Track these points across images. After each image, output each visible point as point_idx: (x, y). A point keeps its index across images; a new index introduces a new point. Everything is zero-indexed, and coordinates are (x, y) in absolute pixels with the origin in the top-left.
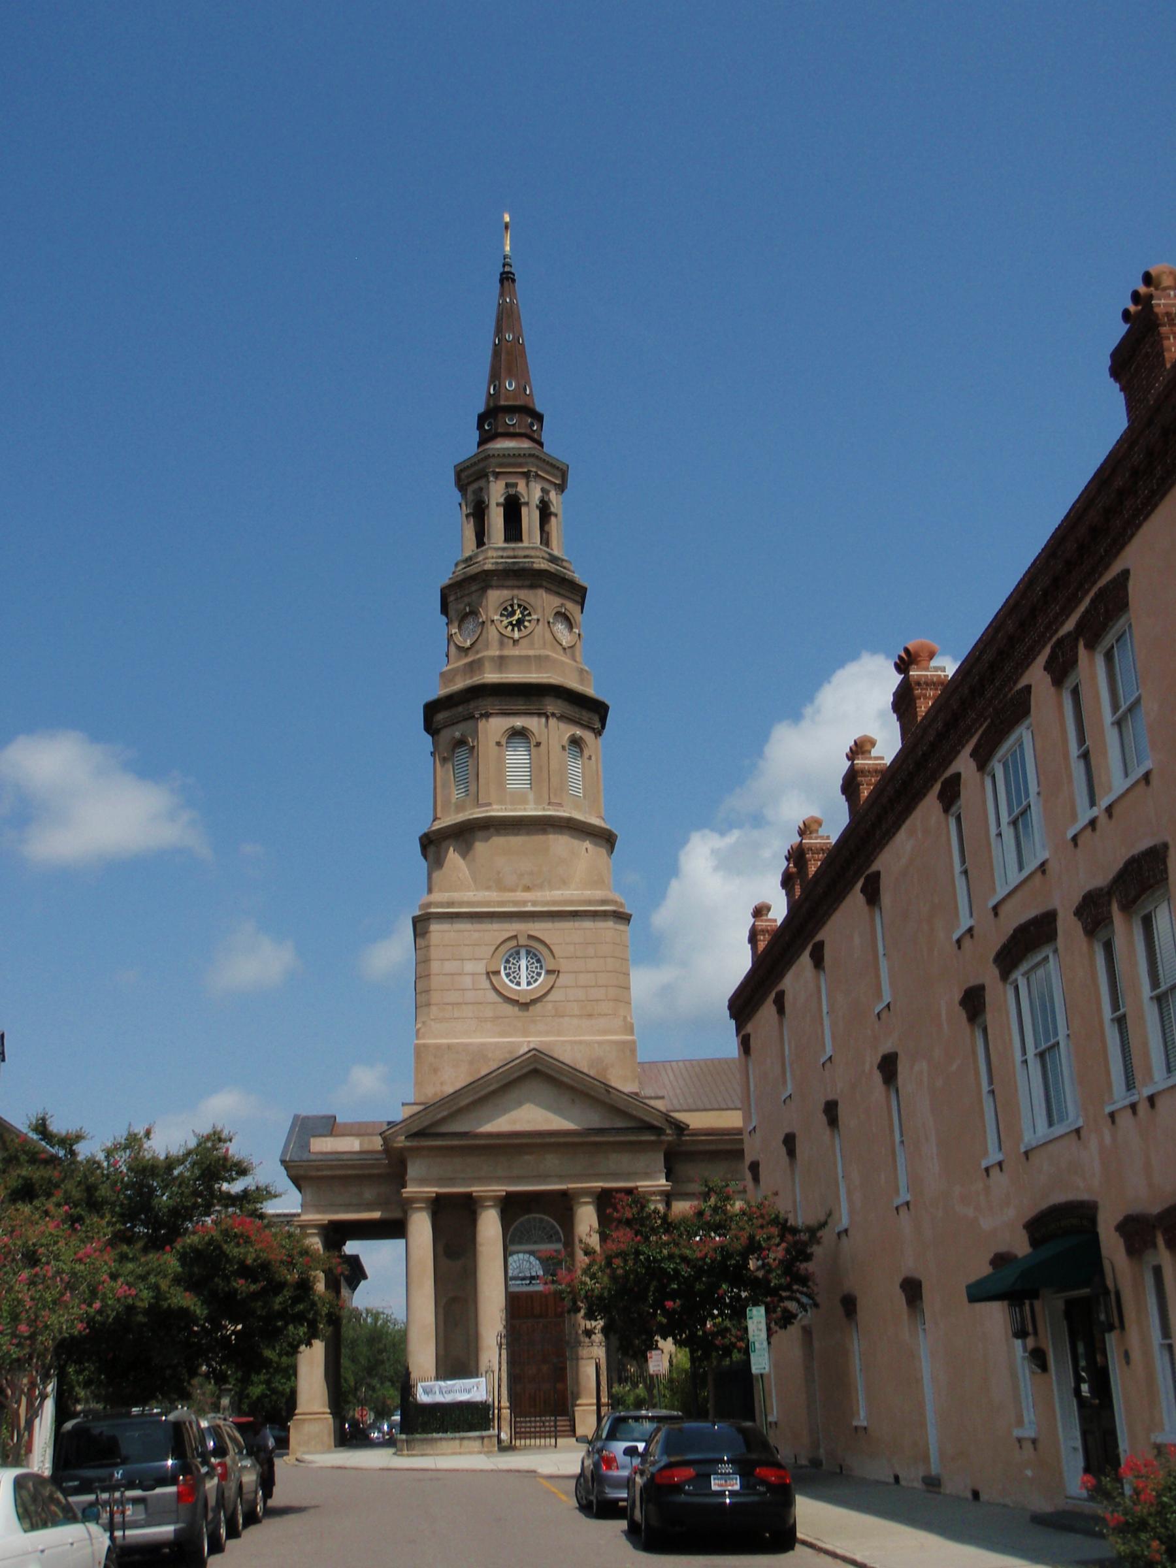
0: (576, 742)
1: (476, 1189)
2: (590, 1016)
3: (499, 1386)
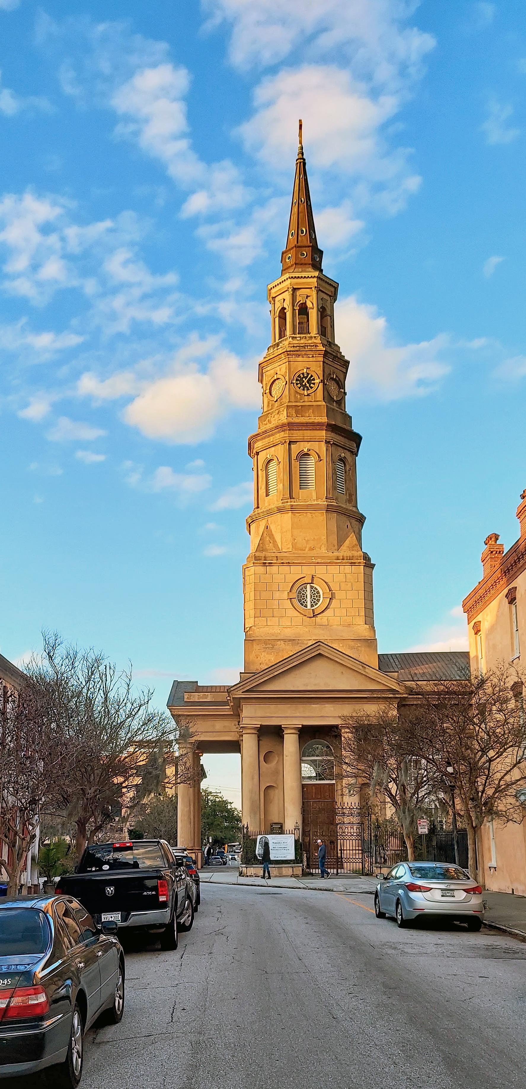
0: (342, 460)
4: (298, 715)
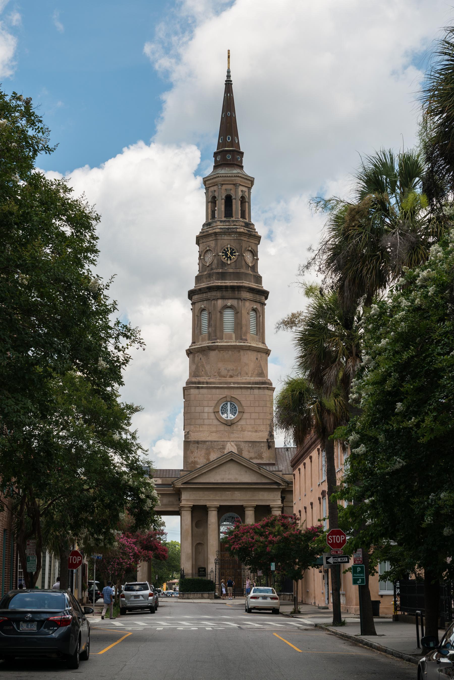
0: (254, 310)
1: (208, 504)
2: (256, 431)
3: (215, 577)
4: (217, 498)
